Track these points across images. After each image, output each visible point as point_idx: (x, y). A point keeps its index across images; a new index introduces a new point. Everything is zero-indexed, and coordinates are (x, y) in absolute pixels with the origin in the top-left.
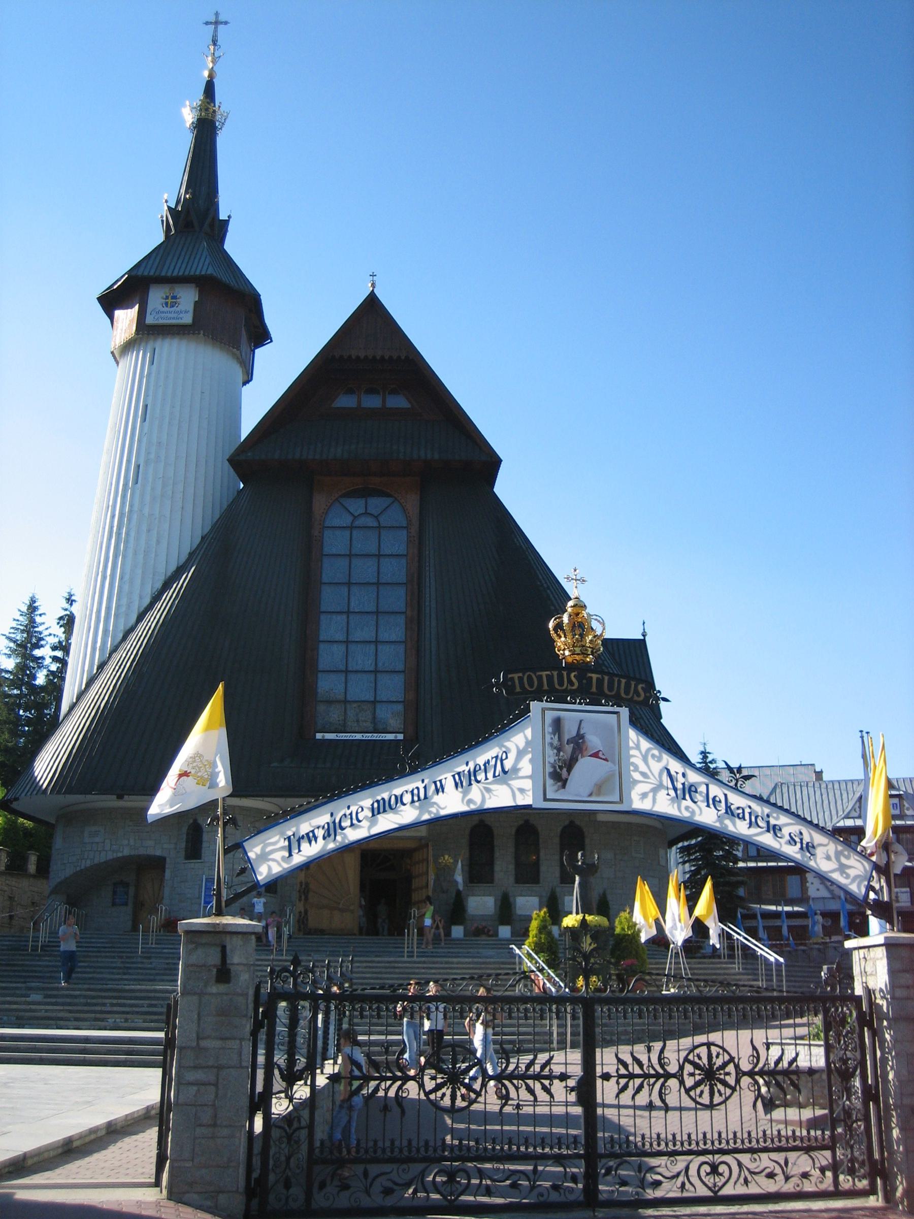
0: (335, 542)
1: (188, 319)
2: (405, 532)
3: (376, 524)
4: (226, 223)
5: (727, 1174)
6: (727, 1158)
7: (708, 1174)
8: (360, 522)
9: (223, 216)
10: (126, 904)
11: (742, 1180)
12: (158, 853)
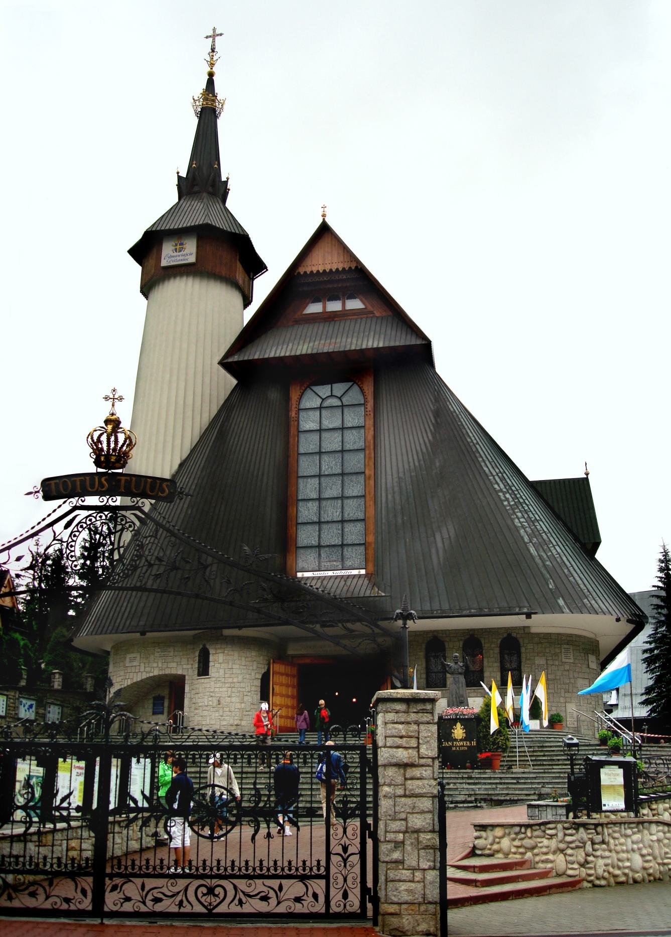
0: (309, 422)
1: (192, 259)
2: (363, 408)
3: (339, 403)
4: (226, 183)
5: (222, 896)
6: (223, 882)
7: (204, 895)
8: (328, 403)
9: (224, 179)
10: (162, 713)
11: (236, 901)
12: (180, 672)
